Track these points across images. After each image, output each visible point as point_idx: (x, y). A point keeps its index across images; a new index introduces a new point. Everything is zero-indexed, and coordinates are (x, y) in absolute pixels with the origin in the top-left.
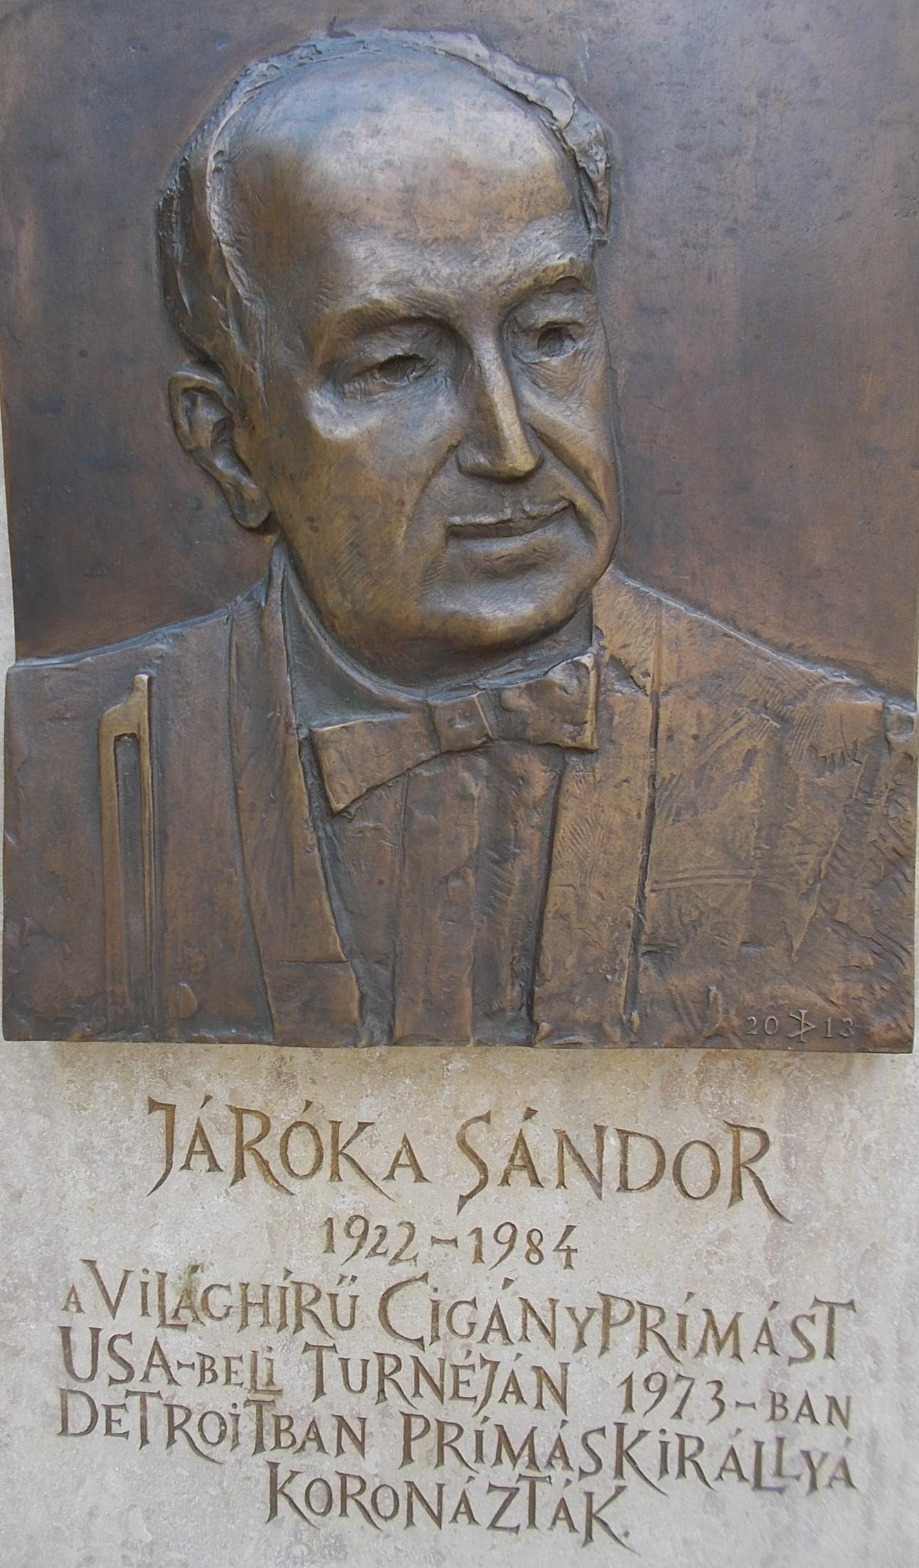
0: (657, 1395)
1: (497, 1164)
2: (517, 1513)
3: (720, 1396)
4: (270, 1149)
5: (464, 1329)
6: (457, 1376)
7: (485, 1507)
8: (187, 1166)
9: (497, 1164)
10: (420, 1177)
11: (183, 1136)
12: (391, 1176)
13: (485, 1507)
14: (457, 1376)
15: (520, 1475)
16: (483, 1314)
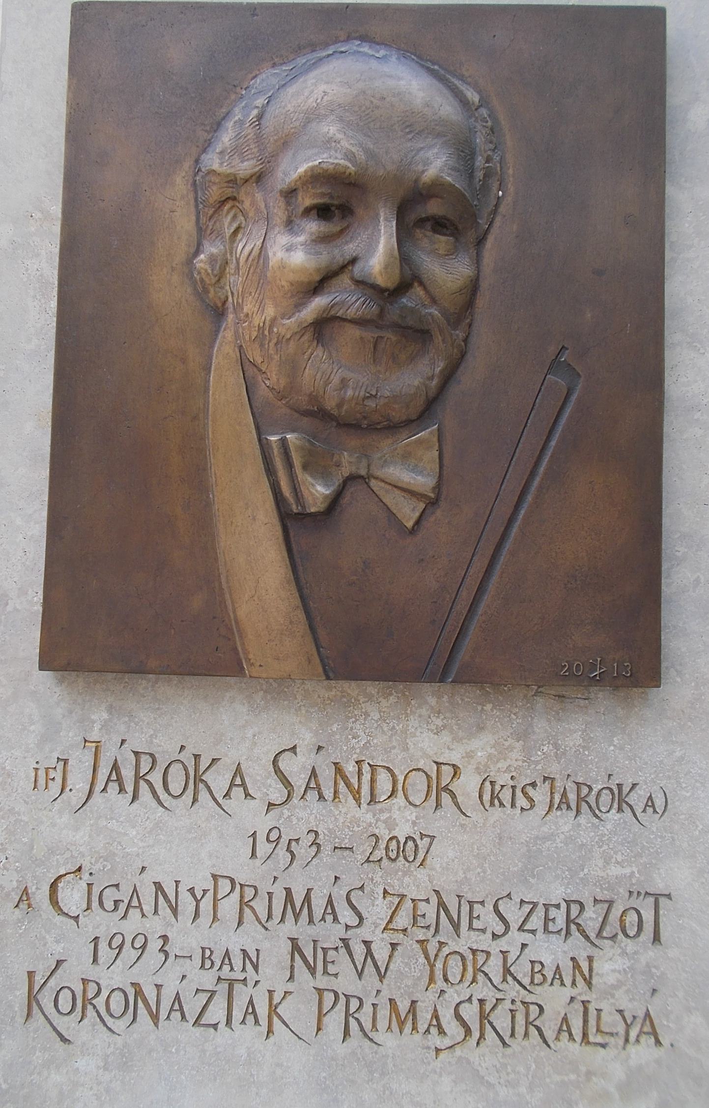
0: (141, 950)
1: (299, 782)
2: (217, 1012)
3: (166, 948)
4: (156, 778)
5: (109, 905)
6: (415, 908)
7: (192, 1006)
8: (104, 790)
9: (299, 782)
10: (247, 795)
11: (104, 772)
12: (227, 795)
13: (192, 1006)
14: (415, 908)
15: (197, 989)
16: (124, 895)
